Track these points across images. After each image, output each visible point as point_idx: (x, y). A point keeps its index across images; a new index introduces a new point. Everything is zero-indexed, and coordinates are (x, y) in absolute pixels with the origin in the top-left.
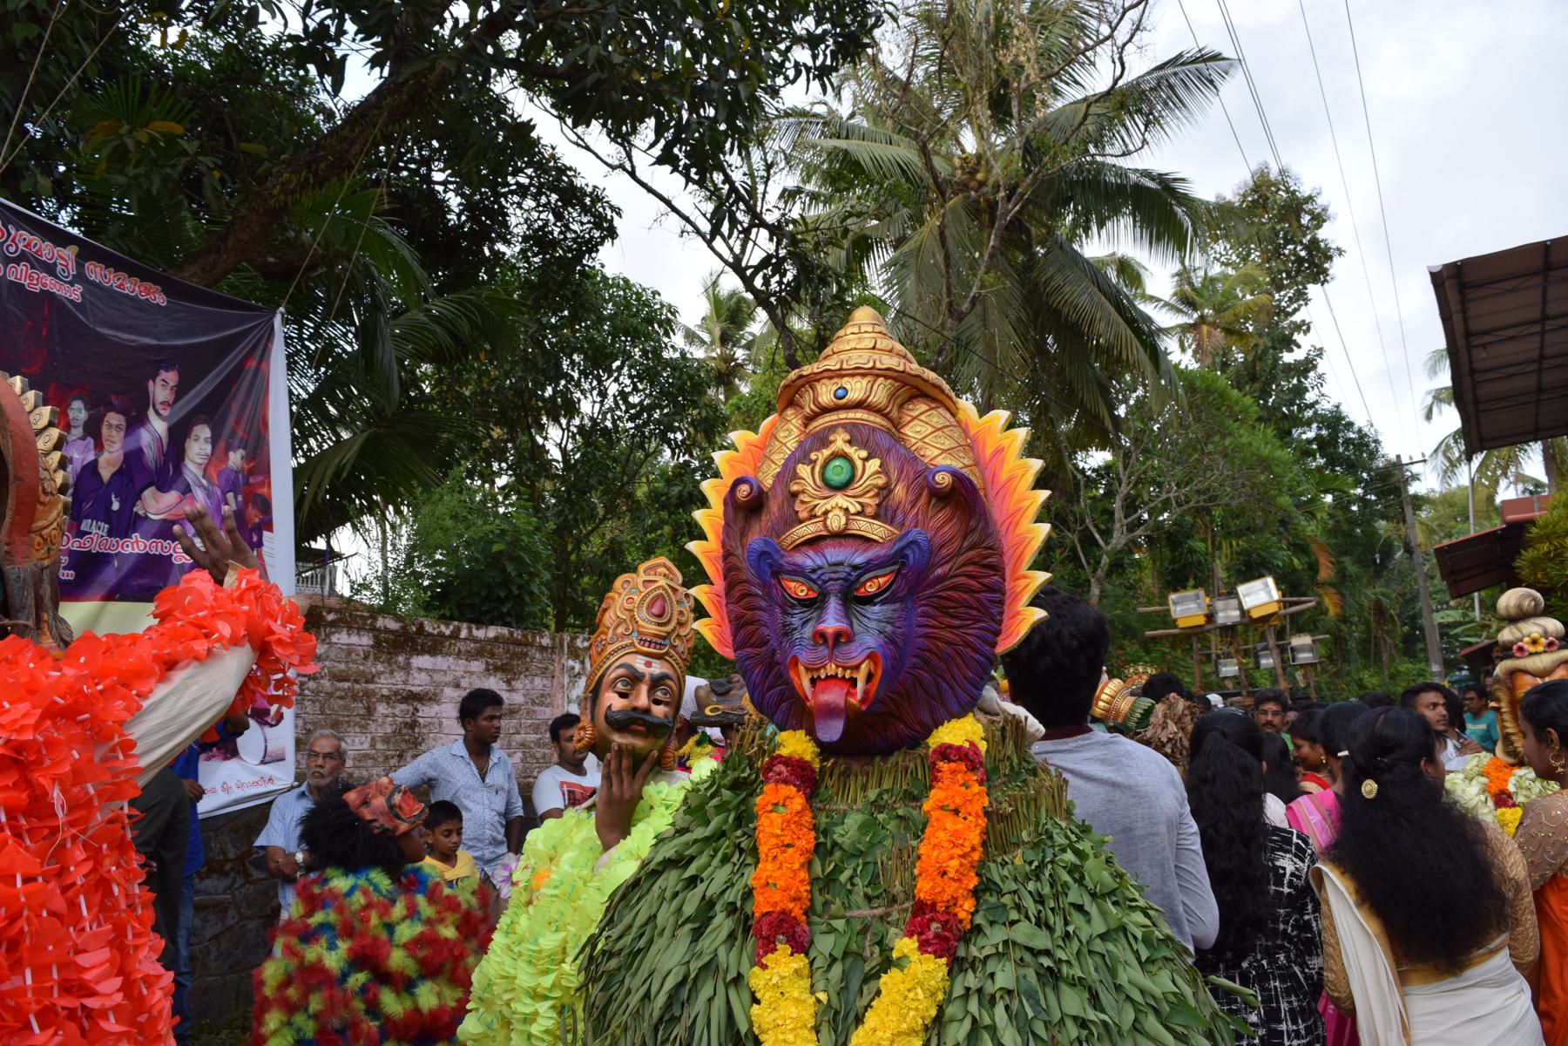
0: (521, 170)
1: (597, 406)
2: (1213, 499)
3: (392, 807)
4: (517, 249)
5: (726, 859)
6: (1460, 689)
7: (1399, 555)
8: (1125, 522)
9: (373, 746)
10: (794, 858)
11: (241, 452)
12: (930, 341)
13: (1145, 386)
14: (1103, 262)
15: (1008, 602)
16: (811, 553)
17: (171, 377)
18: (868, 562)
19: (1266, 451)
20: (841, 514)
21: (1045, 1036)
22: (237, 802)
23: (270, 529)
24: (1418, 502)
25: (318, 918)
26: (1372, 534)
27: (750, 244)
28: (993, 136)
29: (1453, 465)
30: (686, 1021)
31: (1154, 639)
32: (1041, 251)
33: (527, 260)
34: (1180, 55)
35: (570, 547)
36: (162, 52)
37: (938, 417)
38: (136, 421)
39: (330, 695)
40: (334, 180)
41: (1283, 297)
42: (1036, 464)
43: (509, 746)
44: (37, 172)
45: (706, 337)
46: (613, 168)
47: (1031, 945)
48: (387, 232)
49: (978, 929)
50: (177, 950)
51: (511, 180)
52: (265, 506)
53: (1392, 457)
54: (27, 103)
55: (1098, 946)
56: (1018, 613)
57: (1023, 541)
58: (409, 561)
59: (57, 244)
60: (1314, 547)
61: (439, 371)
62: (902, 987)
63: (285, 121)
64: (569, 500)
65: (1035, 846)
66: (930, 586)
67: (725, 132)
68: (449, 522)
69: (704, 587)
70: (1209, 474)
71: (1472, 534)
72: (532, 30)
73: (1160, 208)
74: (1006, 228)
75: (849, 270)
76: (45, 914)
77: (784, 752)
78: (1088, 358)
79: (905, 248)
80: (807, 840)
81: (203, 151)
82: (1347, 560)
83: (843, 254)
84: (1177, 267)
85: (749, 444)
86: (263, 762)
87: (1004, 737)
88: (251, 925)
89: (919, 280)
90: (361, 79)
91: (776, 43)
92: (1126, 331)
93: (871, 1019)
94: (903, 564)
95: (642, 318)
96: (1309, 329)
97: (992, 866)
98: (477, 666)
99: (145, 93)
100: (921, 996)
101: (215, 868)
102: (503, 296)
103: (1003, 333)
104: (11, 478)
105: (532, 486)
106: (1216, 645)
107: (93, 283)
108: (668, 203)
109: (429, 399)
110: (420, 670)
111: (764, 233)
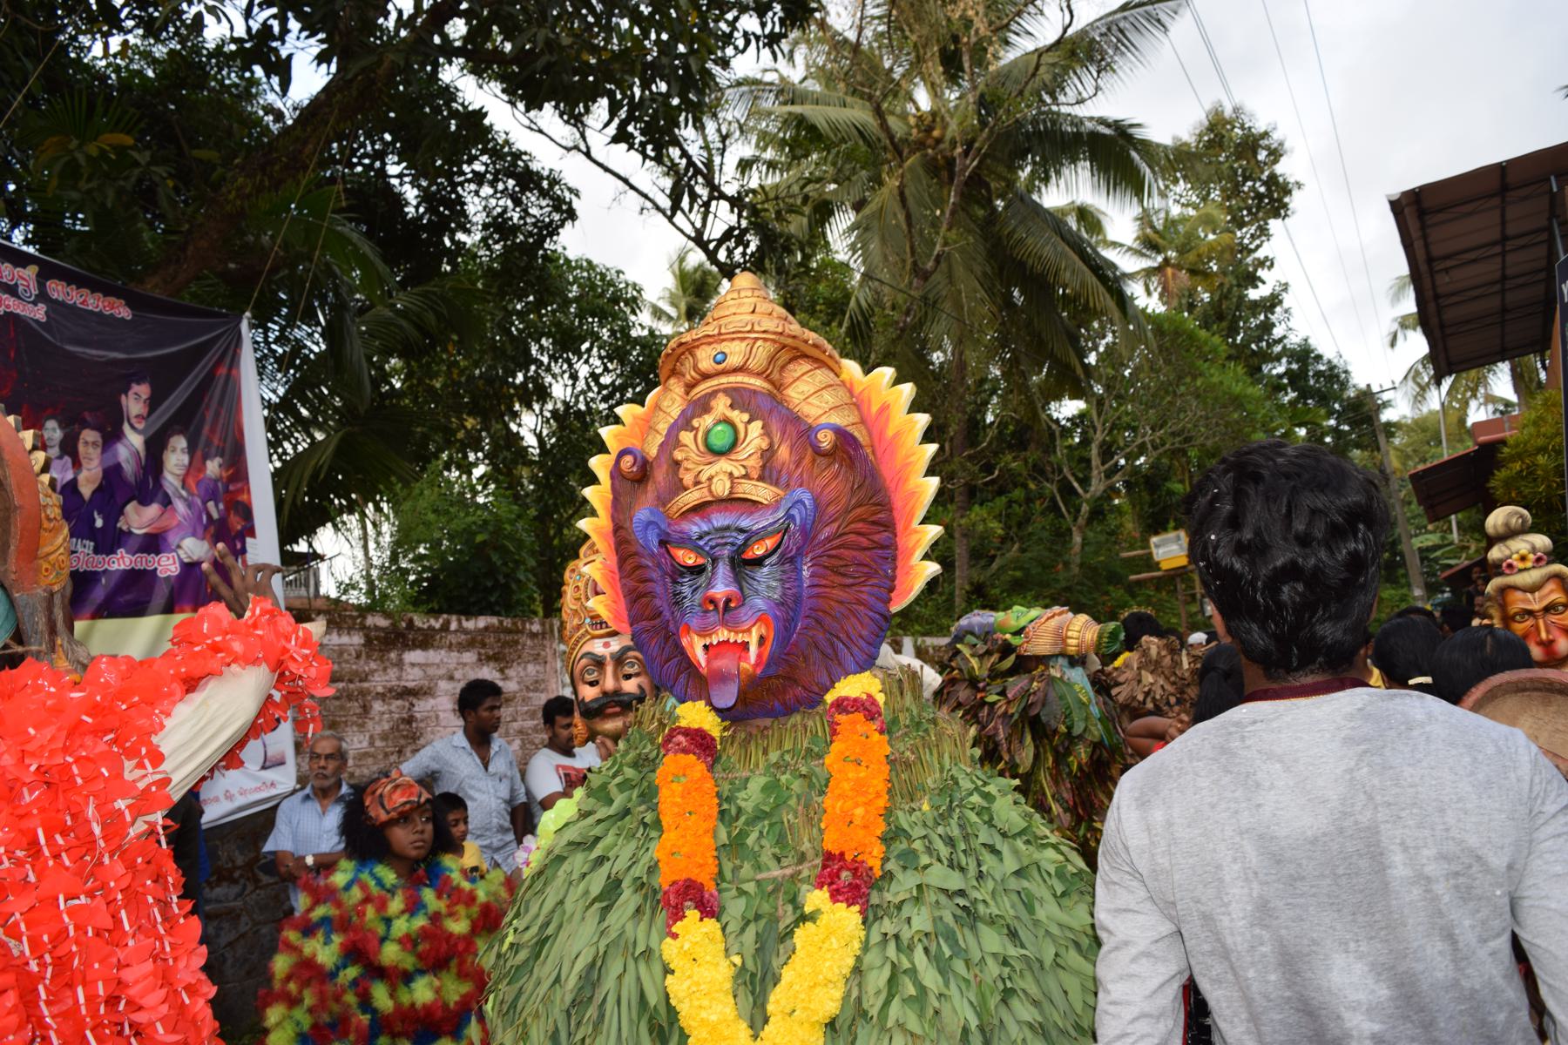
19: (1237, 389)
41: (1245, 234)
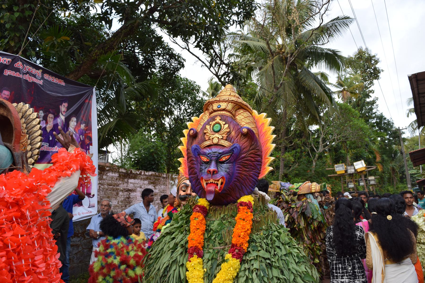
0: (159, 49)
1: (179, 113)
2: (347, 139)
3: (126, 219)
4: (158, 70)
5: (182, 233)
6: (416, 192)
7: (399, 155)
8: (322, 145)
9: (118, 203)
10: (200, 232)
11: (84, 125)
12: (269, 95)
13: (328, 108)
14: (317, 74)
15: (263, 165)
16: (208, 149)
17: (66, 105)
18: (223, 152)
19: (362, 126)
20: (217, 139)
21: (267, 282)
22: (82, 218)
23: (92, 145)
24: (404, 140)
25: (109, 251)
26: (391, 149)
27: (220, 69)
28: (287, 40)
29: (414, 129)
30: (168, 276)
31: (330, 177)
32: (299, 71)
33: (160, 73)
34: (338, 17)
35: (171, 151)
36: (64, 18)
37: (246, 114)
38: (56, 116)
39: (107, 189)
40: (109, 52)
41: (366, 83)
42: (273, 128)
43: (154, 204)
44: (31, 50)
45: (208, 94)
46: (183, 48)
47: (264, 256)
48: (124, 66)
49: (249, 252)
50: (66, 257)
51: (156, 52)
52: (90, 139)
53: (397, 127)
54: (29, 32)
55: (284, 258)
56: (265, 168)
57: (268, 149)
58: (128, 154)
59: (37, 69)
61: (137, 103)
62: (227, 267)
63: (96, 36)
64: (171, 138)
65: (266, 230)
66: (240, 159)
67: (214, 39)
68: (139, 144)
69: (182, 158)
70: (346, 132)
71: (420, 149)
72: (162, 12)
73: (333, 59)
74: (290, 64)
75: (247, 76)
76: (27, 245)
77: (199, 204)
78: (312, 100)
79: (262, 70)
80: (203, 227)
81: (75, 44)
82: (384, 156)
83: (246, 71)
84: (337, 75)
85: (196, 120)
86: (89, 207)
87: (259, 200)
88: (85, 251)
89: (266, 79)
90: (117, 25)
91: (228, 15)
92: (323, 93)
93: (218, 276)
94: (233, 153)
95: (191, 89)
96: (374, 92)
97: (254, 235)
98: (146, 182)
99: (60, 29)
100: (232, 269)
101: (76, 235)
102: (154, 83)
103: (289, 93)
104: (14, 129)
105: (161, 134)
106: (347, 179)
107: (46, 80)
108: (198, 58)
109: (134, 111)
110: (131, 183)
111: (224, 66)
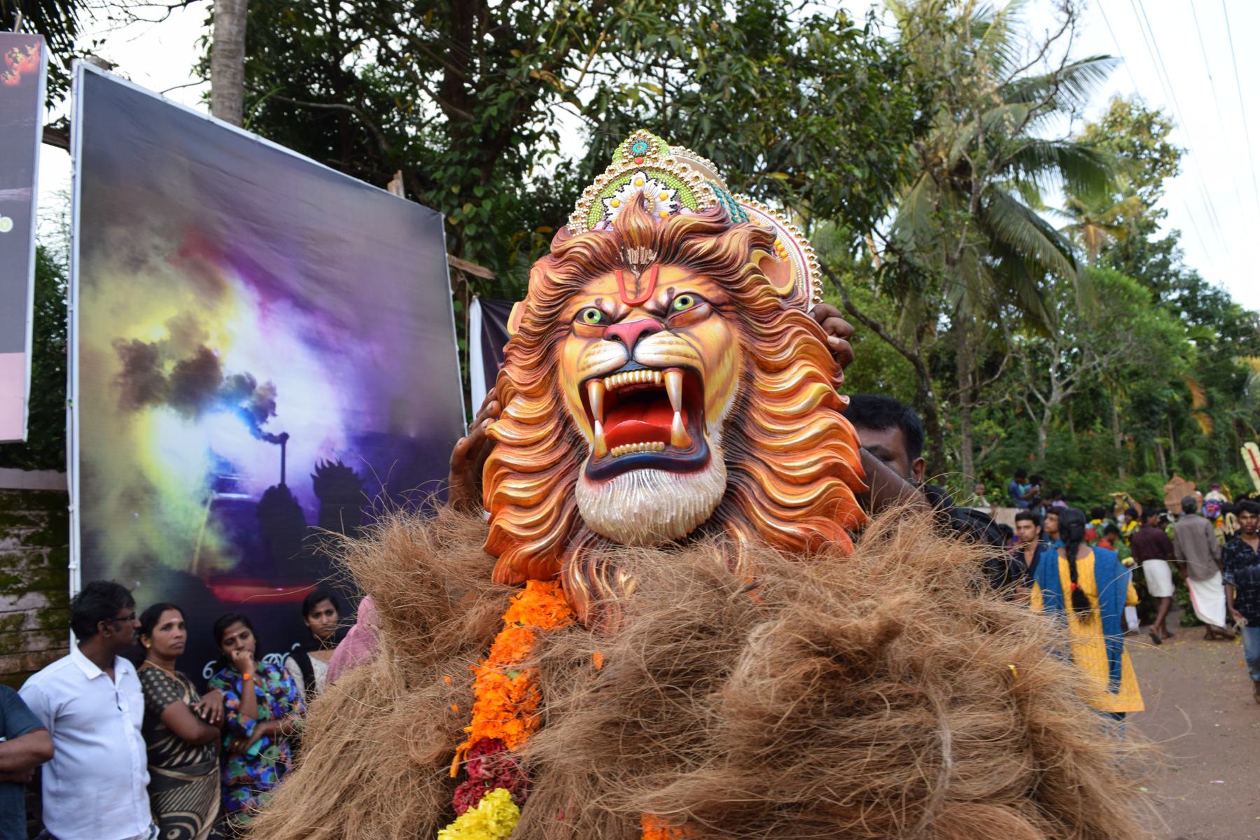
19: (1163, 326)
41: (1144, 191)
60: (1188, 384)
